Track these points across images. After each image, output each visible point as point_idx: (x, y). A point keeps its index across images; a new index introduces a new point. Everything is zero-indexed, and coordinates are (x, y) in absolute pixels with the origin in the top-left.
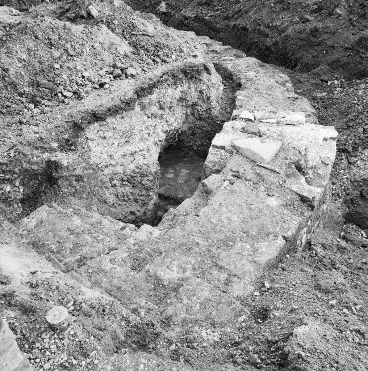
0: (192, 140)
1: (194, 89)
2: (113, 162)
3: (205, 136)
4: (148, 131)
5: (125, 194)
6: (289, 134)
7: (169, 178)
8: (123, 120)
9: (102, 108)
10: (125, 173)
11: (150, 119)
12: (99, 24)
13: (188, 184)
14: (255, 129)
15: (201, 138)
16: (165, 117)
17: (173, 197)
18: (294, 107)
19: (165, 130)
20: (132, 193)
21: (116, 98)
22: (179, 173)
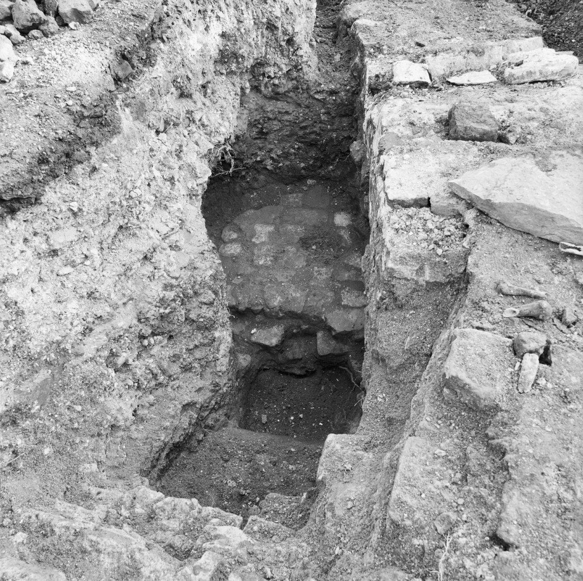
0: (260, 149)
1: (252, 22)
2: (102, 309)
3: (291, 135)
4: (167, 174)
5: (155, 371)
6: (571, 116)
7: (232, 256)
8: (96, 176)
9: (14, 165)
10: (141, 318)
11: (163, 136)
12: (126, 109)
13: (282, 262)
14: (484, 122)
15: (280, 141)
16: (197, 116)
17: (260, 308)
18: (487, 25)
19: (206, 152)
20: (174, 356)
21: (50, 109)
22: (252, 237)
